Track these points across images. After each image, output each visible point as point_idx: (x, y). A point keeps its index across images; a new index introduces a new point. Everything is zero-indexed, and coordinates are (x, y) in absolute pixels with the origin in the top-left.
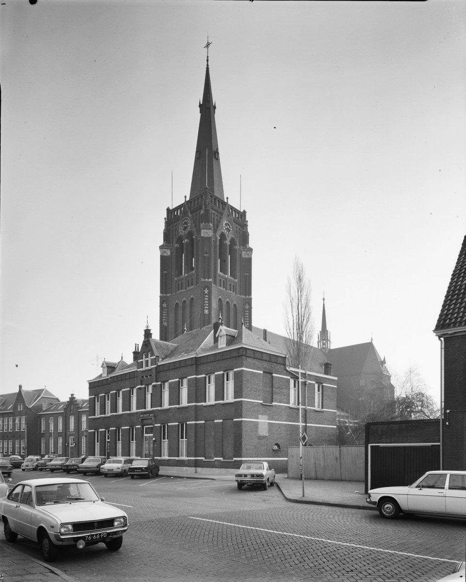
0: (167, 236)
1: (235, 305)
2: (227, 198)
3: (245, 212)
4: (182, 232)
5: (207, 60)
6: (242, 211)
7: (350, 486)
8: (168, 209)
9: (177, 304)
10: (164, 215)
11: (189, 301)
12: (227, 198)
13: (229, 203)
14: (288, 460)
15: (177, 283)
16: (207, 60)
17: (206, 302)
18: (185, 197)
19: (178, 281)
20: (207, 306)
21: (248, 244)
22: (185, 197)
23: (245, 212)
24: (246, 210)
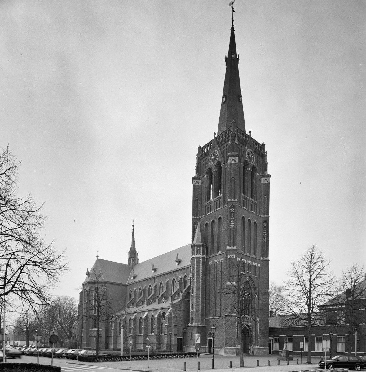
0: (198, 169)
1: (255, 223)
2: (250, 132)
3: (264, 145)
4: (211, 164)
5: (233, 21)
6: (261, 144)
7: (317, 365)
8: (200, 148)
9: (213, 221)
10: (197, 152)
11: (210, 224)
12: (250, 132)
13: (252, 137)
14: (205, 317)
15: (216, 203)
16: (233, 21)
17: (232, 221)
18: (215, 134)
19: (208, 204)
20: (231, 222)
21: (267, 171)
22: (215, 134)
23: (264, 145)
24: (265, 144)
